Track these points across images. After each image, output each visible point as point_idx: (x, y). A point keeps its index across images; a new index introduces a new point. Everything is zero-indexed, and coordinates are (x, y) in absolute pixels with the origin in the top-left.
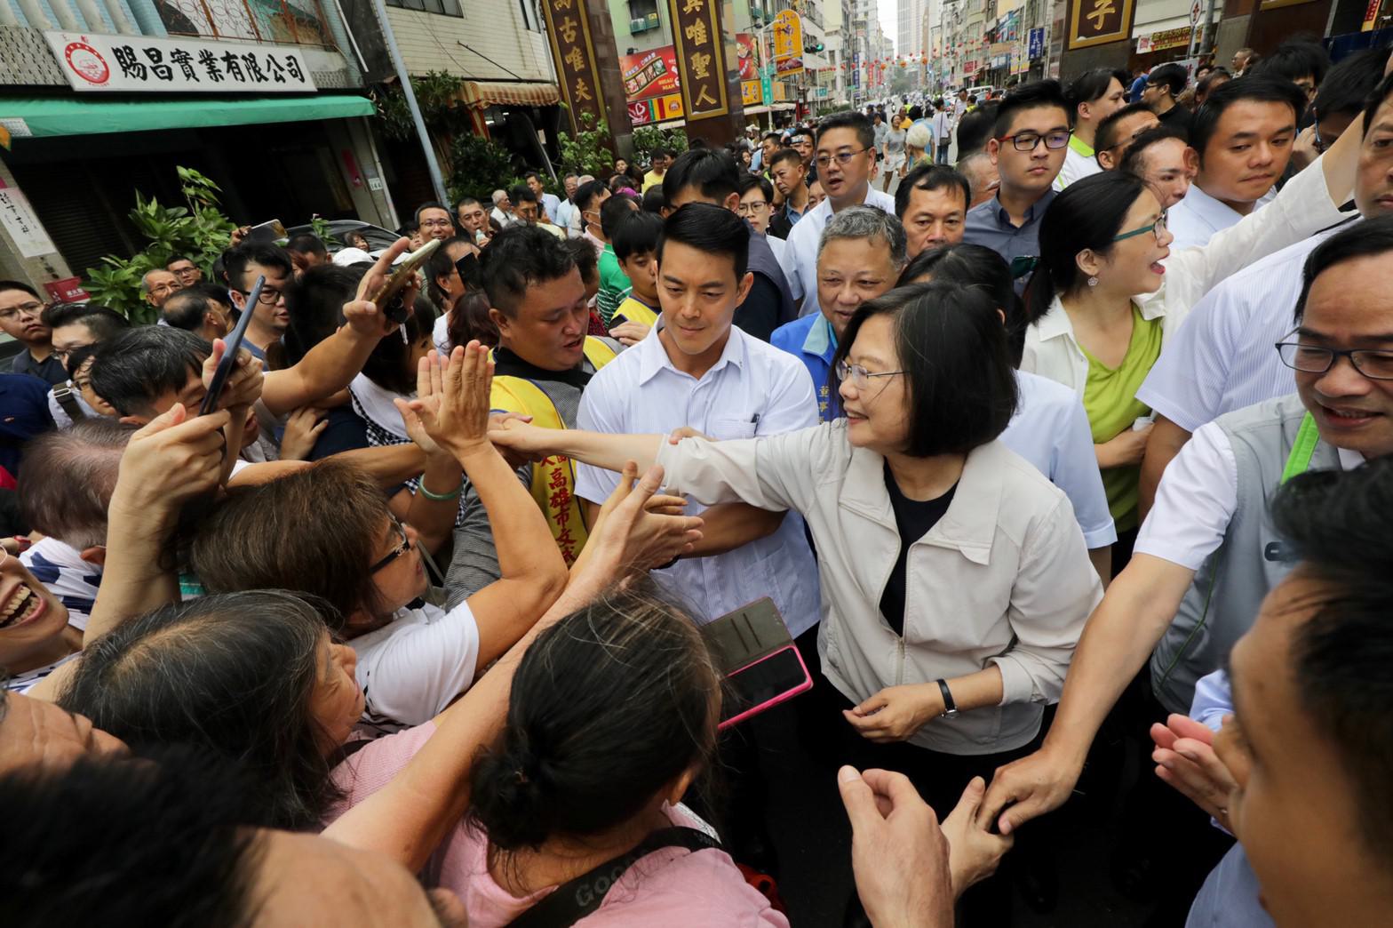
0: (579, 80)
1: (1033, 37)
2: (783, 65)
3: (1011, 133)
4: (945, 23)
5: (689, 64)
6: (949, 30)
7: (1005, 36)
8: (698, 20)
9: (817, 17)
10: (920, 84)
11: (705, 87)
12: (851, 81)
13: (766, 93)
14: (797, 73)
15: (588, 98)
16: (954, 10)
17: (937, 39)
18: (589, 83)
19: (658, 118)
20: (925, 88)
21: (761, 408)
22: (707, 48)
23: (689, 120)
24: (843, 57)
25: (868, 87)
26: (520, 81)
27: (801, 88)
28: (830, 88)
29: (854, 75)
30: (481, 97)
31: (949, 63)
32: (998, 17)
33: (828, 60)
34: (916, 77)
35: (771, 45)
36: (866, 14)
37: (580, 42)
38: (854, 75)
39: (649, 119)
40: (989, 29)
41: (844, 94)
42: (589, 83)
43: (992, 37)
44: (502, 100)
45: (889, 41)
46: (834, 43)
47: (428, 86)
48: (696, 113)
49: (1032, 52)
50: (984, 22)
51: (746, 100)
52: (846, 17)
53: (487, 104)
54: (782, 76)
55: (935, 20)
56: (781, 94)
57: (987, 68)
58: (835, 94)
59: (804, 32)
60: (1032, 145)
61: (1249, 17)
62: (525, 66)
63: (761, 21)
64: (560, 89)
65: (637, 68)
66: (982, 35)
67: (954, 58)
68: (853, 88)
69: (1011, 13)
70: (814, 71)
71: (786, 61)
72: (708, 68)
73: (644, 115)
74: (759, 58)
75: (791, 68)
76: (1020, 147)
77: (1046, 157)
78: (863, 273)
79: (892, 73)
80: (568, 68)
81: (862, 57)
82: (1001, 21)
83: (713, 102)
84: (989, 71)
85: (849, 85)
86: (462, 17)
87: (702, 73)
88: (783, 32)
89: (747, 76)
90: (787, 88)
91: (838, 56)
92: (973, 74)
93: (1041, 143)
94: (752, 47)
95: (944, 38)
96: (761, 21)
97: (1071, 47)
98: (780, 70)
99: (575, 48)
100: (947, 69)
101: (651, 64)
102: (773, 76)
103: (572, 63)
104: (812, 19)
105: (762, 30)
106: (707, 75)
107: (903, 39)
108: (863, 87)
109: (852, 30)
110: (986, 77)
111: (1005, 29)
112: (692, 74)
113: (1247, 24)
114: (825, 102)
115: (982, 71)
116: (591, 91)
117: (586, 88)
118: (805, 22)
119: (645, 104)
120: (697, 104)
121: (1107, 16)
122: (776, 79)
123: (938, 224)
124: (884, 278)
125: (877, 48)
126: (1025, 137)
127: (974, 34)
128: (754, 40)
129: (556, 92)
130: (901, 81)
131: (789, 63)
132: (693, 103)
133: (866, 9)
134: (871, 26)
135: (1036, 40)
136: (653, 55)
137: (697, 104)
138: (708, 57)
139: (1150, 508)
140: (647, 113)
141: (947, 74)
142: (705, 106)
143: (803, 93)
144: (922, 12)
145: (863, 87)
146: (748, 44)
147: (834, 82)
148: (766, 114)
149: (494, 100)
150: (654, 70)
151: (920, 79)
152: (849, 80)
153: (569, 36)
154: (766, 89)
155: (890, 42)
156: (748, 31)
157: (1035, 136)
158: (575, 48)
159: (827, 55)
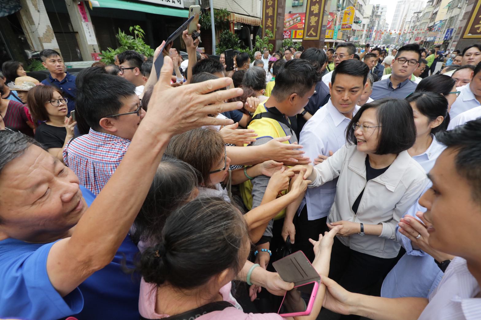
0: (269, 19)
2: (344, 26)
5: (309, 19)
6: (413, 24)
7: (436, 29)
8: (317, 4)
9: (362, 11)
10: (395, 42)
11: (313, 29)
14: (348, 30)
15: (271, 25)
16: (417, 16)
18: (273, 21)
19: (293, 37)
22: (317, 15)
23: (304, 39)
25: (374, 40)
26: (249, 16)
27: (348, 36)
28: (359, 38)
30: (235, 19)
32: (435, 21)
33: (362, 27)
35: (341, 18)
37: (273, 6)
39: (290, 37)
40: (430, 26)
42: (273, 21)
43: (430, 29)
44: (241, 21)
45: (387, 24)
46: (366, 22)
47: (218, 12)
49: (446, 37)
50: (429, 23)
51: (327, 36)
52: (373, 12)
53: (236, 21)
55: (408, 19)
56: (340, 37)
58: (361, 40)
60: (404, 62)
62: (252, 11)
63: (340, 9)
64: (262, 21)
65: (291, 18)
66: (426, 27)
68: (368, 39)
69: (441, 21)
71: (346, 25)
72: (316, 22)
73: (289, 35)
74: (336, 22)
77: (406, 67)
79: (385, 36)
80: (267, 14)
82: (436, 24)
83: (314, 34)
84: (425, 42)
85: (367, 38)
87: (313, 23)
88: (347, 14)
89: (329, 28)
90: (343, 35)
91: (366, 26)
93: (407, 63)
94: (334, 17)
96: (340, 9)
98: (342, 28)
99: (271, 7)
101: (296, 18)
102: (339, 29)
103: (268, 13)
104: (360, 11)
106: (315, 24)
107: (393, 24)
108: (372, 40)
109: (374, 18)
110: (423, 44)
111: (437, 27)
112: (309, 23)
115: (422, 41)
116: (273, 24)
117: (271, 22)
118: (357, 12)
119: (290, 32)
120: (308, 34)
122: (340, 31)
126: (403, 59)
128: (336, 15)
129: (260, 21)
130: (388, 40)
132: (307, 33)
133: (382, 11)
134: (382, 17)
135: (449, 33)
136: (298, 15)
137: (308, 34)
138: (317, 18)
140: (290, 35)
141: (408, 40)
142: (311, 35)
143: (349, 38)
144: (404, 15)
145: (372, 40)
147: (362, 36)
149: (239, 21)
150: (297, 20)
151: (396, 40)
152: (368, 36)
153: (270, 3)
154: (335, 34)
155: (388, 24)
156: (334, 12)
157: (406, 60)
158: (271, 7)
159: (362, 25)
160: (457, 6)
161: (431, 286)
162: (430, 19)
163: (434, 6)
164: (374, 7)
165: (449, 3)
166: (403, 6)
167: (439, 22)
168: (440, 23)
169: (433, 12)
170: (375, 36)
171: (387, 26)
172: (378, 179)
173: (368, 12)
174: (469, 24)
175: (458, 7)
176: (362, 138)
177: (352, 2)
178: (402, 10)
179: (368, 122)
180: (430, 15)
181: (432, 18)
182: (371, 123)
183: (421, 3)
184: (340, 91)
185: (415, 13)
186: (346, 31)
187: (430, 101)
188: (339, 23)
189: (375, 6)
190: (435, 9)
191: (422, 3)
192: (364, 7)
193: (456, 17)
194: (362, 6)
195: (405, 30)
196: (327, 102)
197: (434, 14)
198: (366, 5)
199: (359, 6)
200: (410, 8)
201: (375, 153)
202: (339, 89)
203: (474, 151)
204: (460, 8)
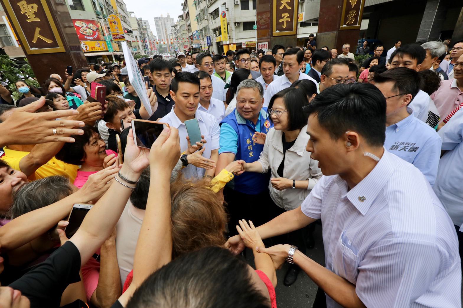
1: (207, 39)
2: (115, 36)
3: (240, 59)
4: (173, 33)
5: (17, 10)
6: (175, 35)
10: (168, 51)
11: (38, 30)
12: (145, 47)
13: (110, 47)
16: (175, 29)
20: (170, 52)
21: (232, 161)
24: (141, 39)
28: (137, 49)
29: (146, 46)
31: (177, 45)
35: (108, 28)
36: (146, 26)
38: (146, 46)
40: (190, 35)
41: (143, 51)
43: (191, 38)
45: (155, 36)
50: (187, 33)
52: (139, 25)
57: (191, 47)
59: (123, 27)
67: (179, 44)
68: (146, 49)
70: (130, 42)
71: (117, 35)
72: (36, 14)
74: (103, 32)
76: (242, 62)
78: (252, 99)
81: (147, 40)
82: (194, 33)
83: (49, 41)
84: (192, 49)
85: (145, 48)
86: (390, 149)
87: (32, 18)
88: (113, 23)
91: (138, 38)
92: (187, 49)
93: (246, 61)
95: (174, 37)
98: (114, 38)
100: (177, 47)
107: (159, 36)
108: (150, 50)
113: (334, 35)
114: (137, 53)
118: (122, 22)
120: (34, 42)
121: (287, 22)
122: (113, 42)
123: (207, 88)
124: (258, 101)
125: (152, 38)
133: (145, 25)
134: (148, 30)
139: (155, 141)
141: (177, 48)
142: (40, 44)
145: (150, 50)
147: (139, 46)
148: (111, 55)
152: (144, 47)
156: (95, 20)
159: (134, 37)
160: (204, 19)
162: (187, 30)
163: (185, 20)
164: (137, 20)
165: (196, 17)
166: (160, 22)
167: (195, 32)
168: (197, 32)
170: (150, 46)
171: (155, 38)
172: (291, 149)
175: (205, 19)
176: (277, 120)
177: (112, 11)
179: (279, 108)
180: (186, 28)
181: (189, 29)
182: (281, 109)
183: (171, 20)
184: (186, 97)
185: (172, 26)
187: (306, 84)
188: (108, 33)
189: (138, 19)
191: (172, 19)
192: (127, 18)
193: (207, 27)
194: (125, 17)
196: (170, 112)
197: (188, 26)
201: (288, 130)
202: (186, 95)
203: (324, 112)
204: (207, 20)
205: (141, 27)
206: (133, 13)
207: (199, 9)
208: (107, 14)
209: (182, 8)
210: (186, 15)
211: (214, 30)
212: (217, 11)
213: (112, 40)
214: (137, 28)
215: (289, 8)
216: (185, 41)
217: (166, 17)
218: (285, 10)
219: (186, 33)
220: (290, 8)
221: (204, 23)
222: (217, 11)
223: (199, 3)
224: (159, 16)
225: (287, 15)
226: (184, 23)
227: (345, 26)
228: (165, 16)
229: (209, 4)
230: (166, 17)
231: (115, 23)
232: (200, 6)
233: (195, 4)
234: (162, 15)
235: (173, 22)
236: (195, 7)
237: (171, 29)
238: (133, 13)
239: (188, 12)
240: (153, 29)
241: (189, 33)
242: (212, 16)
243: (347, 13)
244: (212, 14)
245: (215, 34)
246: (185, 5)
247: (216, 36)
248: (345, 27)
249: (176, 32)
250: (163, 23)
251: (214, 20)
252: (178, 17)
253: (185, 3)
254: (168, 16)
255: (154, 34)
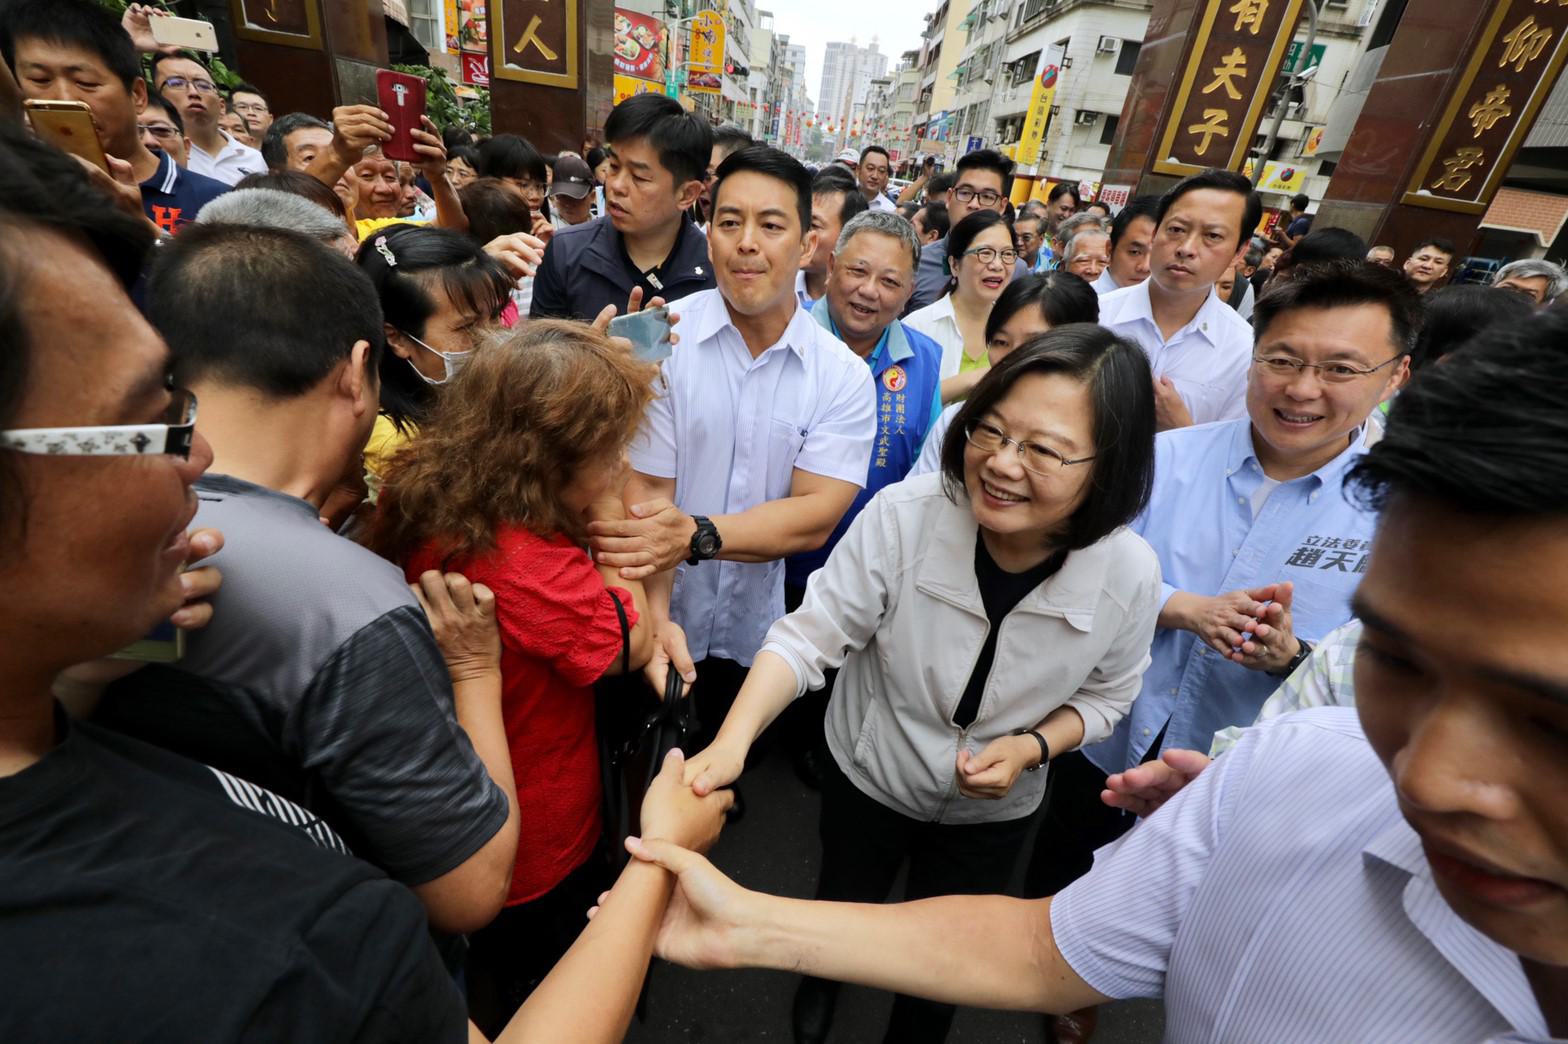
4: (869, 102)
11: (536, 22)
16: (881, 92)
17: (859, 117)
23: (497, 76)
24: (765, 100)
27: (714, 116)
33: (749, 97)
34: (832, 149)
35: (685, 49)
36: (793, 64)
40: (918, 122)
43: (921, 131)
48: (512, 66)
50: (914, 114)
52: (774, 57)
54: (693, 91)
55: (860, 96)
57: (911, 162)
61: (1382, 207)
66: (910, 126)
69: (945, 113)
70: (732, 102)
71: (702, 74)
74: (667, 57)
75: (705, 85)
79: (809, 136)
81: (783, 108)
82: (933, 118)
83: (550, 56)
84: (912, 166)
85: (766, 133)
91: (759, 96)
94: (660, 39)
97: (1156, 169)
98: (692, 82)
102: (682, 87)
105: (677, 22)
107: (823, 105)
110: (908, 172)
113: (1376, 217)
115: (904, 165)
118: (729, 39)
121: (1216, 137)
122: (685, 92)
127: (900, 122)
128: (664, 31)
130: (816, 148)
131: (704, 78)
133: (793, 59)
134: (796, 78)
137: (518, 50)
142: (531, 59)
146: (656, 33)
152: (767, 128)
155: (812, 104)
156: (659, 17)
159: (748, 91)
160: (982, 77)
161: (1051, 929)
162: (915, 102)
163: (920, 69)
164: (774, 41)
166: (840, 59)
167: (940, 115)
169: (921, 84)
173: (760, 56)
174: (1452, 103)
175: (986, 78)
178: (839, 67)
180: (915, 94)
183: (879, 61)
185: (873, 82)
186: (706, 99)
188: (679, 64)
189: (777, 38)
190: (925, 77)
191: (882, 60)
193: (984, 107)
194: (743, 25)
195: (855, 123)
197: (924, 91)
198: (752, 26)
199: (733, 21)
200: (859, 68)
204: (989, 82)
205: (778, 63)
206: (769, 15)
207: (977, 44)
208: (695, 6)
209: (926, 29)
210: (931, 53)
211: (1003, 123)
212: (1032, 59)
213: (682, 87)
214: (765, 66)
215: (1235, 95)
216: (897, 139)
217: (867, 47)
218: (1219, 99)
219: (910, 113)
220: (1239, 97)
221: (978, 92)
222: (1032, 59)
223: (983, 24)
224: (845, 39)
225: (1222, 115)
226: (913, 77)
227: (1425, 193)
228: (863, 44)
229: (1016, 31)
230: (867, 47)
231: (707, 36)
232: (982, 35)
233: (971, 25)
234: (853, 40)
235: (881, 69)
236: (966, 33)
237: (867, 89)
238: (769, 15)
239: (938, 47)
240: (811, 80)
241: (918, 113)
242: (1012, 74)
243: (1448, 150)
244: (1012, 66)
245: (999, 135)
246: (937, 22)
247: (1002, 142)
248: (1422, 197)
249: (879, 101)
250: (849, 68)
251: (1013, 87)
252: (902, 53)
253: (938, 14)
254: (874, 47)
255: (809, 95)
